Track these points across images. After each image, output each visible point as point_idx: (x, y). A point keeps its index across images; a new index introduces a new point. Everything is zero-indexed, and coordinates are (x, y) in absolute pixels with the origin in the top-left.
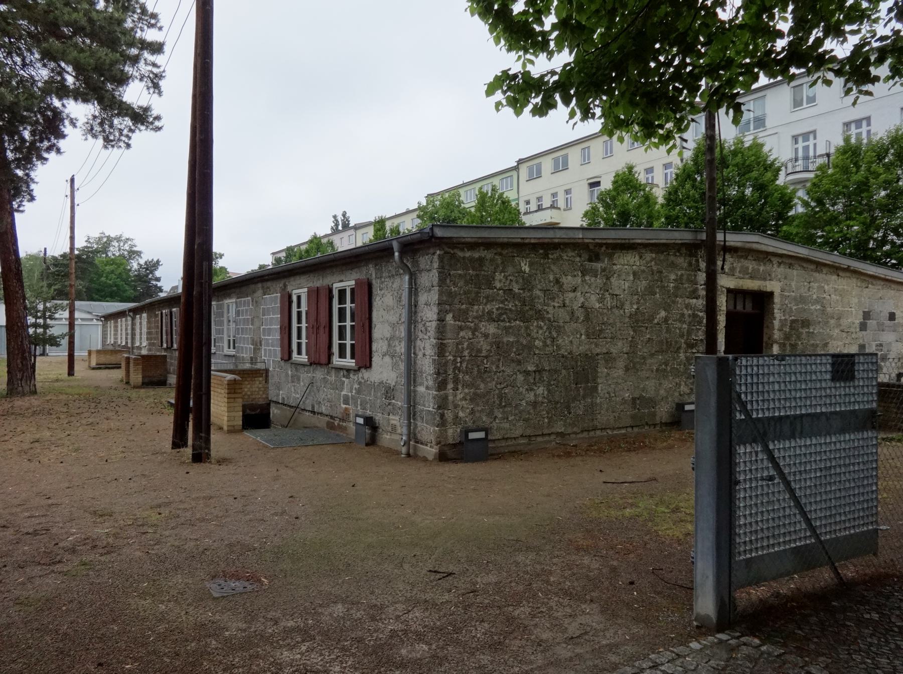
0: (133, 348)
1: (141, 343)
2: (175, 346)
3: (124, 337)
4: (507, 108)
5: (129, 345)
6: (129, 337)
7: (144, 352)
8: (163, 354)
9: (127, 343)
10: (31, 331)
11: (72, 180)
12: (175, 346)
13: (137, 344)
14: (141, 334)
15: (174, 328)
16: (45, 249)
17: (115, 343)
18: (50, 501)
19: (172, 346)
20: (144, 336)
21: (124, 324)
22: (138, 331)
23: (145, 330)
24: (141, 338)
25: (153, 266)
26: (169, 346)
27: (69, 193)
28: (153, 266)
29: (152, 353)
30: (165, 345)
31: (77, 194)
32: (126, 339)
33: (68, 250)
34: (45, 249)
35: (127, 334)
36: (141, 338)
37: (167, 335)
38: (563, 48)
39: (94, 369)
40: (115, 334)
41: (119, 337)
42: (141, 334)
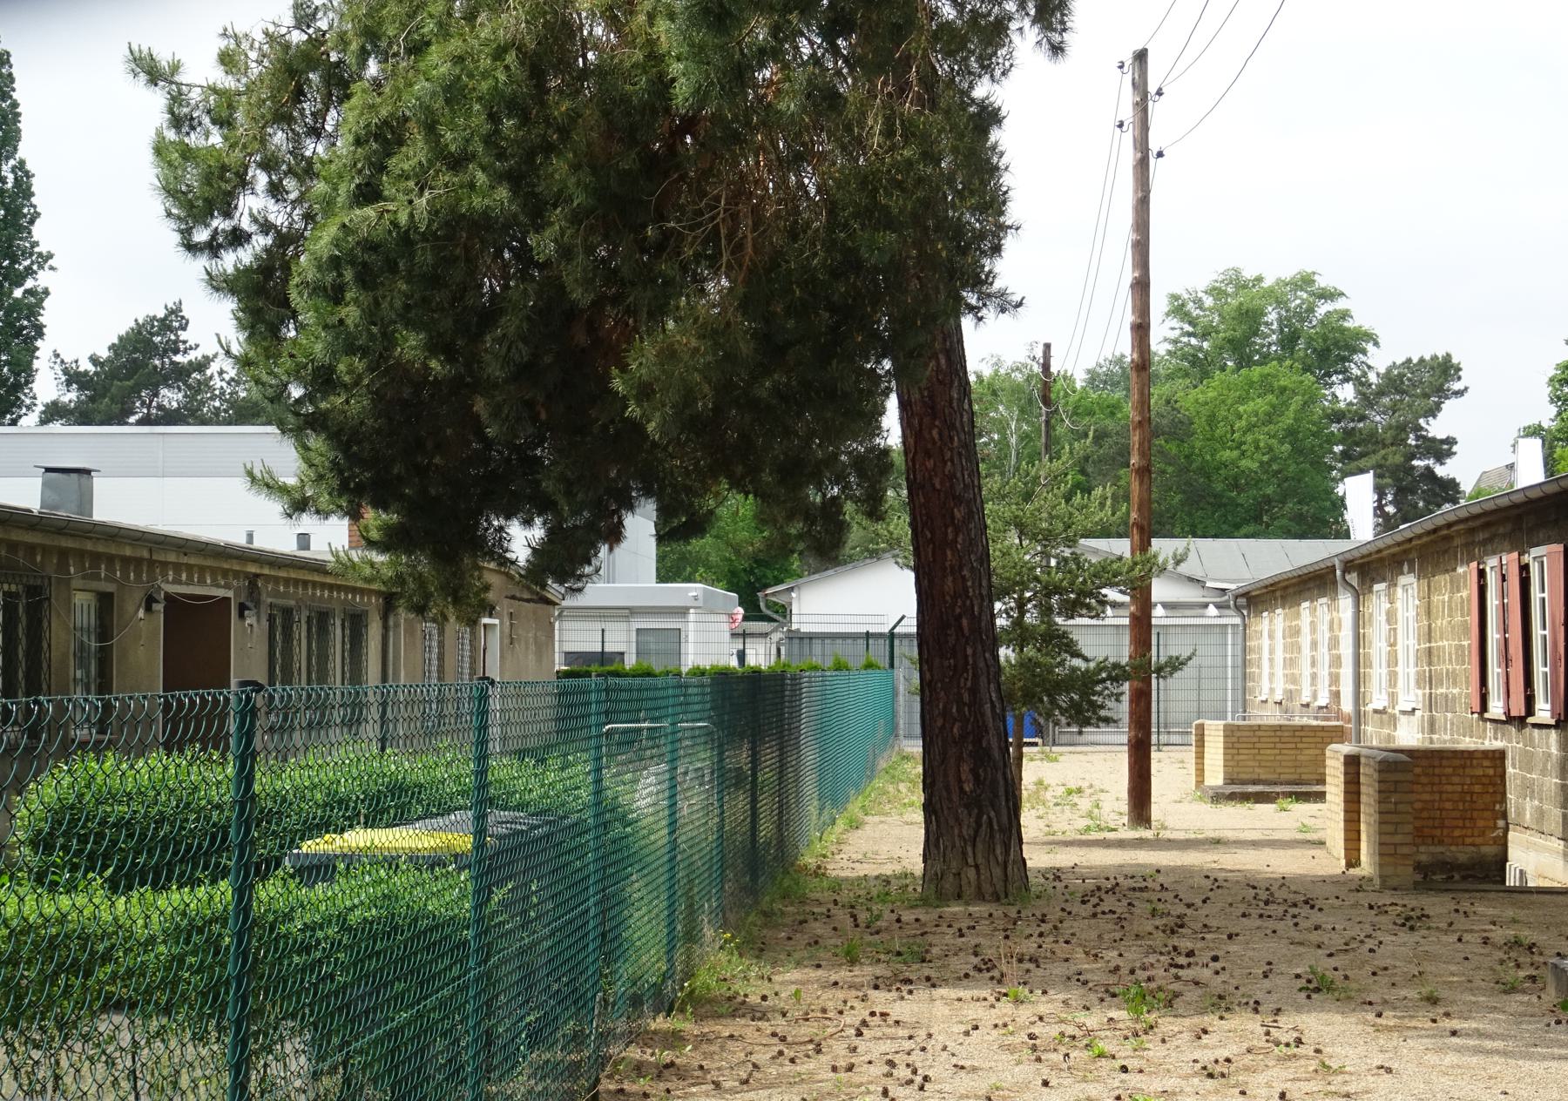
0: (1359, 716)
1: (1393, 698)
2: (1544, 711)
3: (1324, 673)
4: (1339, 871)
5: (1347, 706)
6: (1347, 672)
7: (1409, 735)
8: (1491, 743)
9: (1336, 695)
10: (1006, 653)
11: (1141, 57)
12: (1544, 711)
13: (1377, 700)
14: (1393, 660)
15: (1537, 632)
16: (1047, 347)
17: (1290, 695)
18: (1329, 1088)
19: (1530, 710)
20: (1408, 670)
21: (1327, 617)
22: (1377, 647)
23: (1409, 643)
24: (1393, 678)
25: (1436, 379)
26: (1518, 709)
27: (1127, 113)
28: (1436, 379)
29: (1444, 740)
30: (1496, 709)
31: (1156, 110)
32: (1335, 679)
33: (1125, 347)
34: (1047, 347)
35: (1336, 661)
36: (1393, 678)
37: (1506, 660)
38: (1395, 382)
39: (1218, 797)
40: (1290, 663)
41: (1306, 671)
42: (1393, 660)
